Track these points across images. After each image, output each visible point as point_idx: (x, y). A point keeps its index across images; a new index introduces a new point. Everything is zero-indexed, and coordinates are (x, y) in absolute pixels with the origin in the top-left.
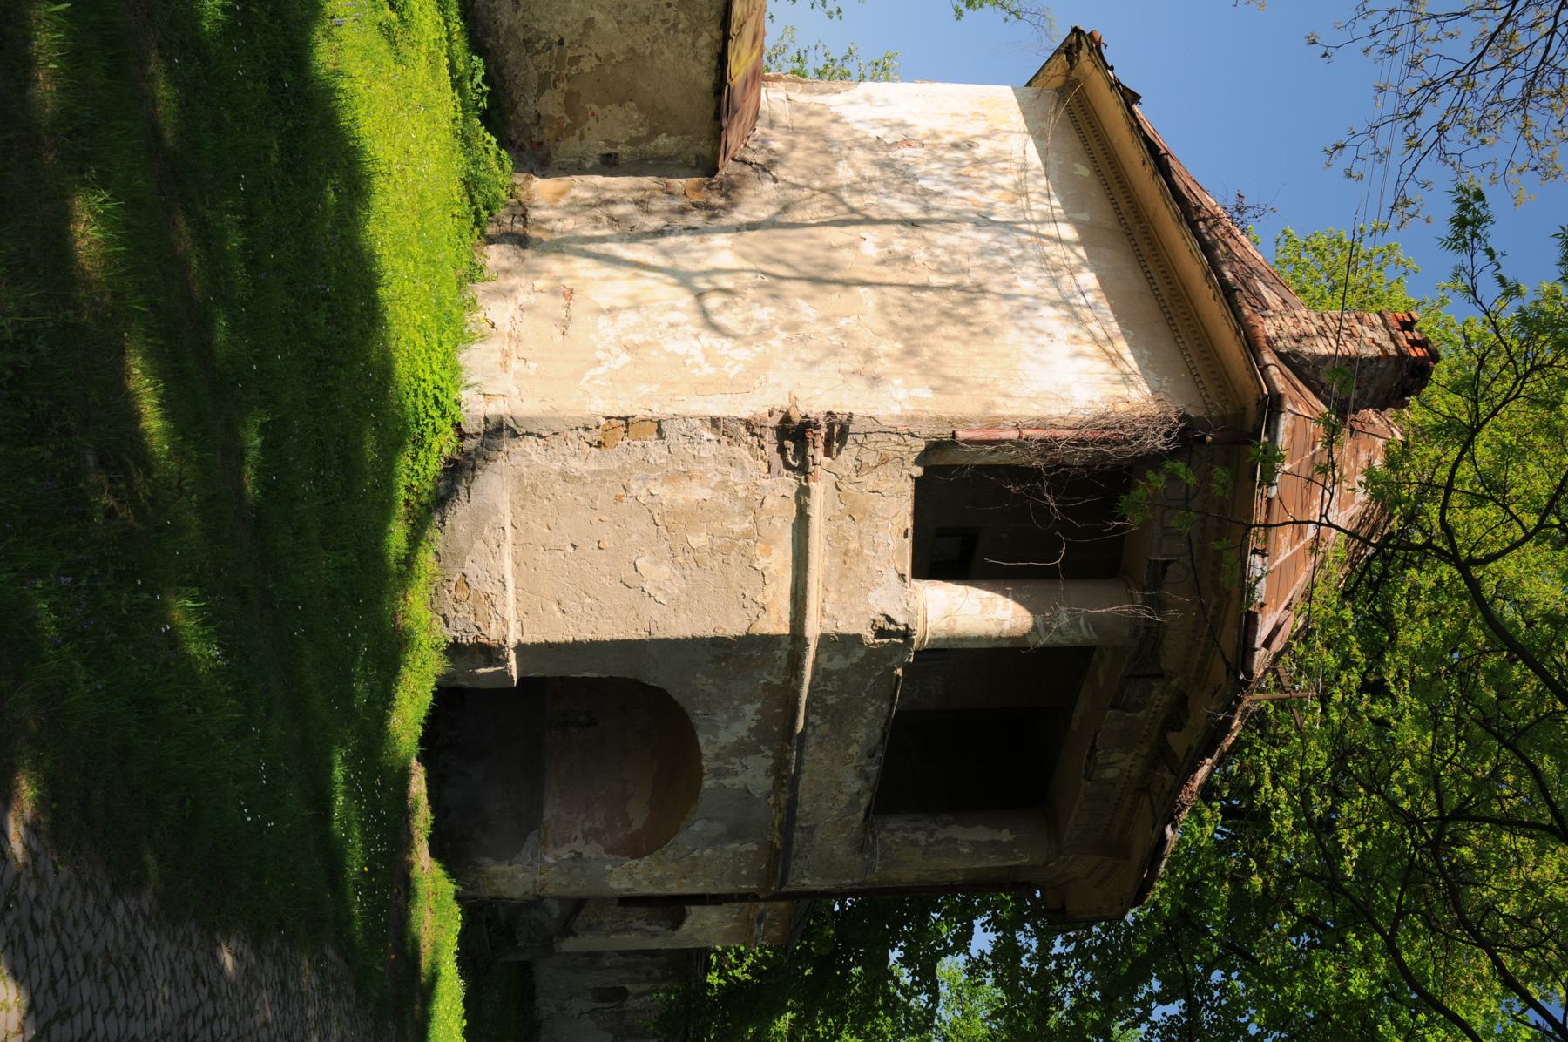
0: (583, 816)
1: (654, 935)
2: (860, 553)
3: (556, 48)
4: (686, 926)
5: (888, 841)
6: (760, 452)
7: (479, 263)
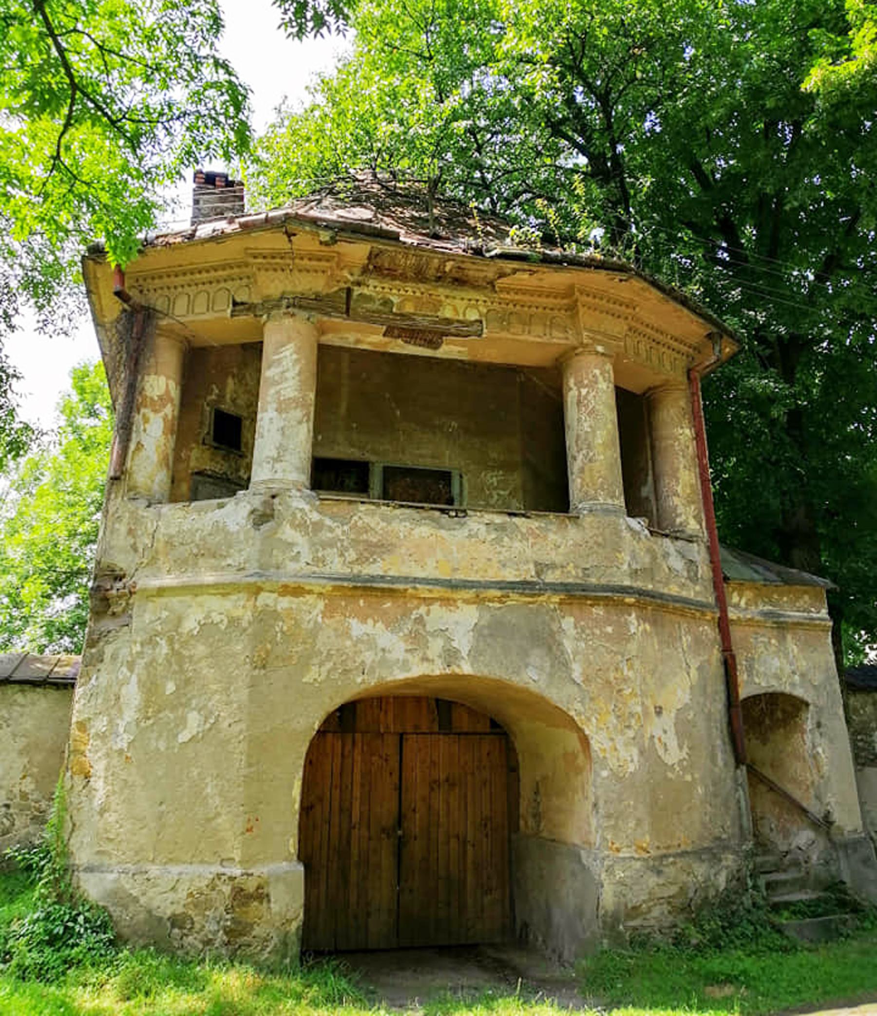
3: (11, 811)
4: (799, 692)
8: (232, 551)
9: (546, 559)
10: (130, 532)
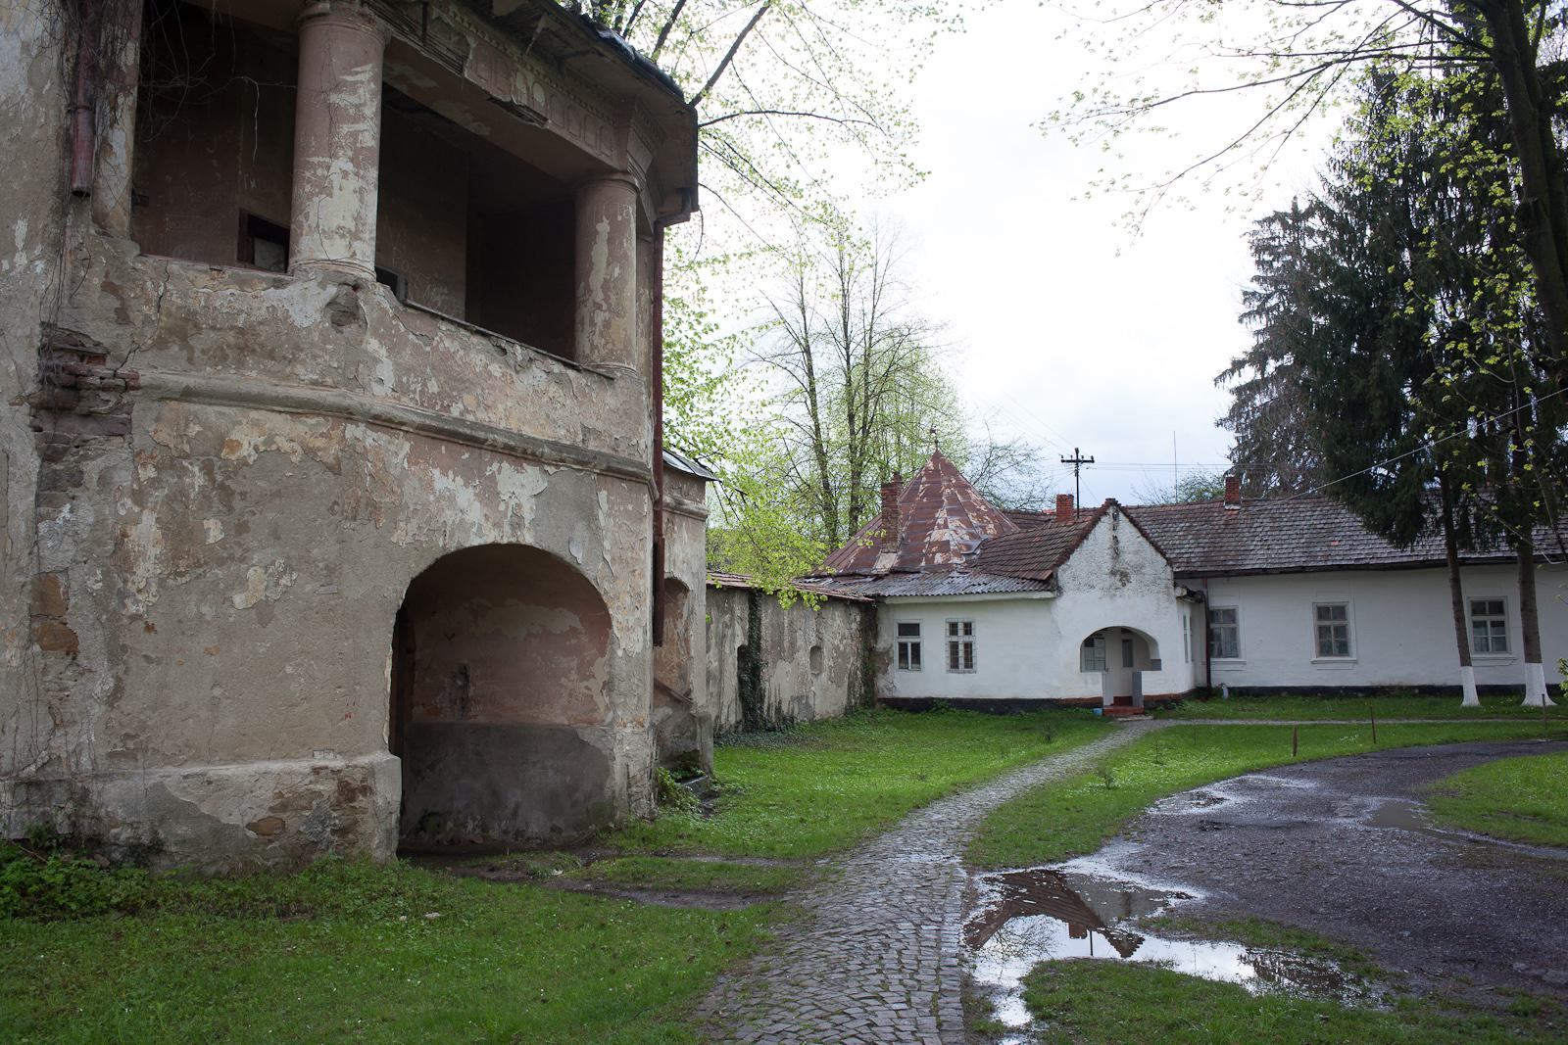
0: (563, 681)
1: (692, 612)
2: (241, 331)
4: (686, 579)
5: (603, 352)
6: (94, 445)
7: (867, 653)
8: (302, 355)
9: (590, 423)
10: (109, 287)
